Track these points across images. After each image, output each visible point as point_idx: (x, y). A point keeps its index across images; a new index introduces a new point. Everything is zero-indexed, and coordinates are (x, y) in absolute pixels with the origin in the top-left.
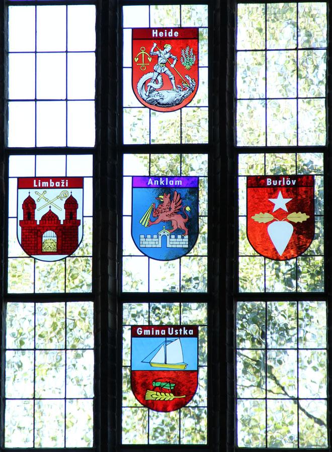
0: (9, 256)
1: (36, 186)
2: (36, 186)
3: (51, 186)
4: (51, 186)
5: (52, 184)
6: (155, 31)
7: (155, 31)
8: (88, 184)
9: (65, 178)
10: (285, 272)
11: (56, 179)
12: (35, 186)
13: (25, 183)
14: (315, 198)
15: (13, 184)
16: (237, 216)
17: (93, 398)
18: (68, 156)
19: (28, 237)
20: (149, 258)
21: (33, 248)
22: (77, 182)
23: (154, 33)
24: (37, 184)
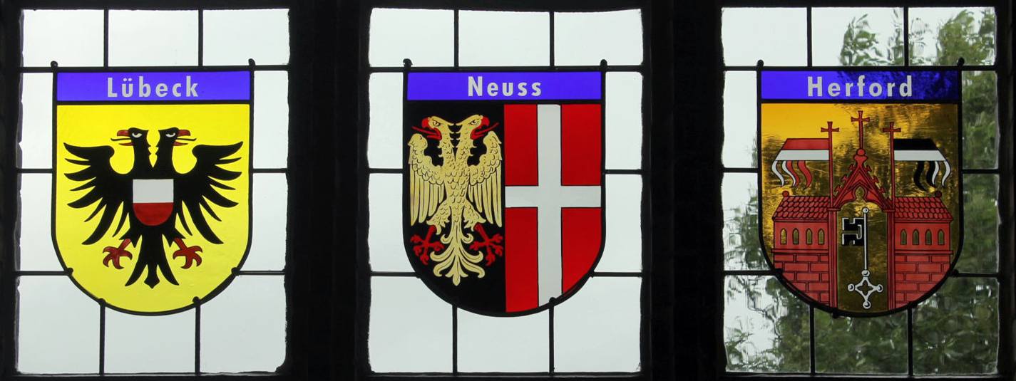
0: (639, 280)
1: (115, 95)
2: (115, 95)
3: (141, 94)
4: (141, 94)
5: (145, 89)
6: (815, 90)
7: (815, 90)
8: (273, 93)
9: (200, 71)
10: (929, 33)
11: (154, 73)
12: (111, 94)
13: (76, 85)
14: (843, 317)
15: (36, 93)
16: (716, 171)
17: (837, 308)
18: (638, 179)
19: (816, 277)
20: (103, 304)
21: (825, 277)
22: (231, 84)
23: (811, 86)
24: (117, 88)
